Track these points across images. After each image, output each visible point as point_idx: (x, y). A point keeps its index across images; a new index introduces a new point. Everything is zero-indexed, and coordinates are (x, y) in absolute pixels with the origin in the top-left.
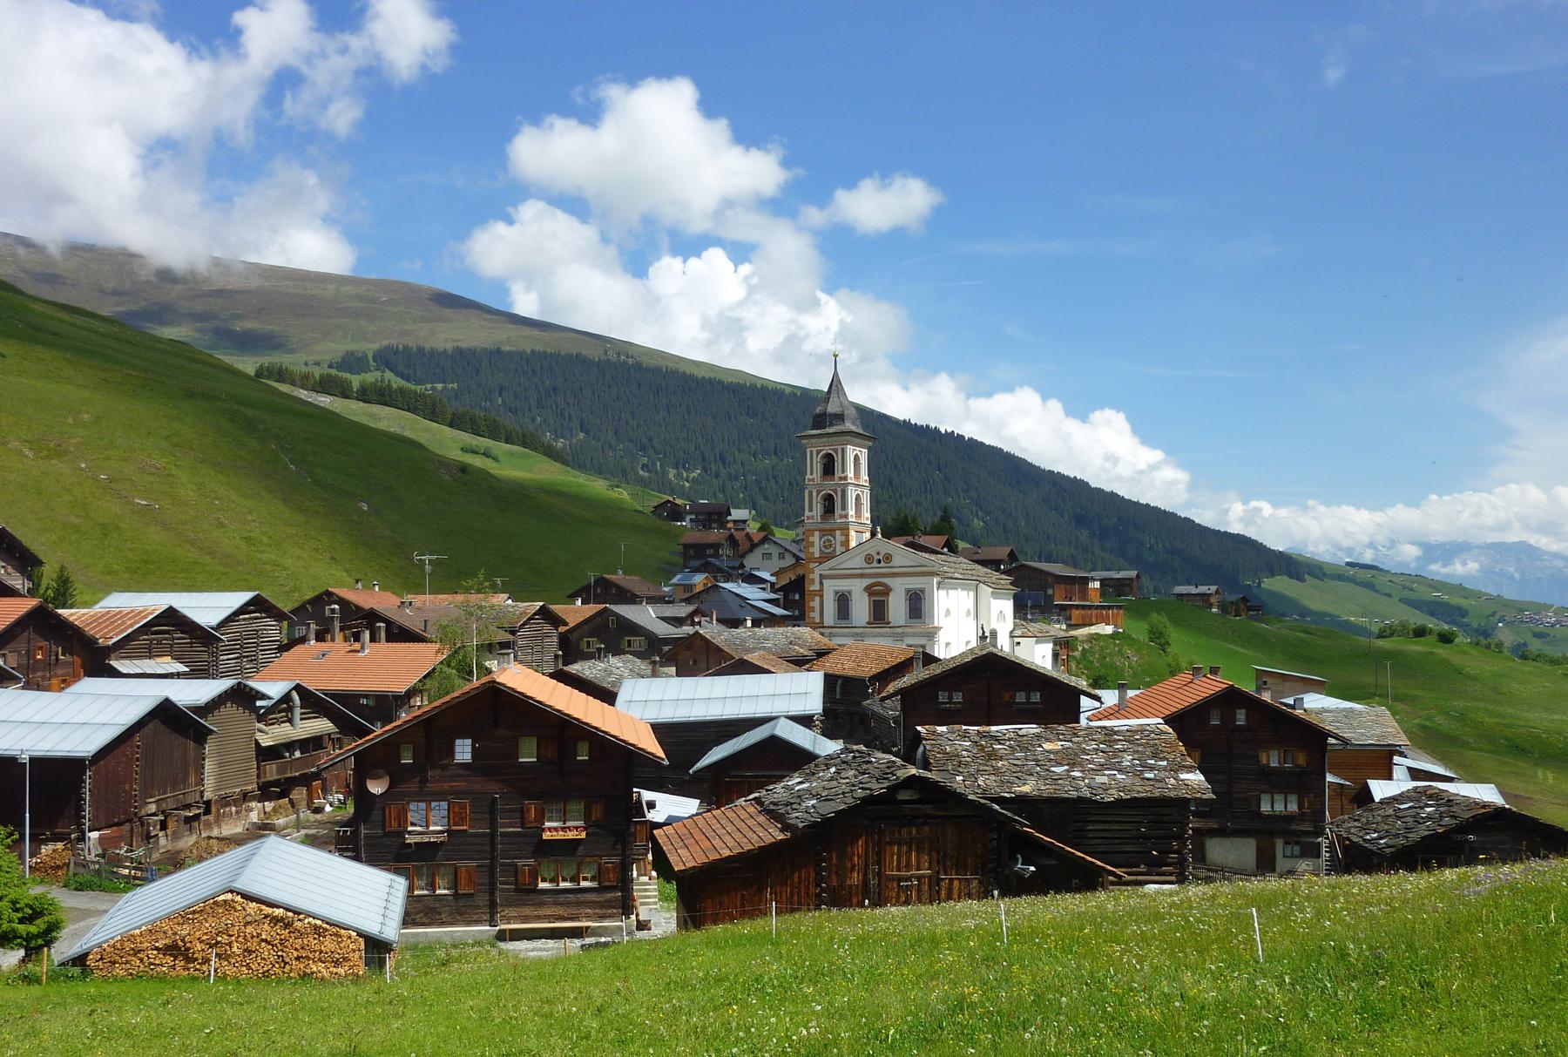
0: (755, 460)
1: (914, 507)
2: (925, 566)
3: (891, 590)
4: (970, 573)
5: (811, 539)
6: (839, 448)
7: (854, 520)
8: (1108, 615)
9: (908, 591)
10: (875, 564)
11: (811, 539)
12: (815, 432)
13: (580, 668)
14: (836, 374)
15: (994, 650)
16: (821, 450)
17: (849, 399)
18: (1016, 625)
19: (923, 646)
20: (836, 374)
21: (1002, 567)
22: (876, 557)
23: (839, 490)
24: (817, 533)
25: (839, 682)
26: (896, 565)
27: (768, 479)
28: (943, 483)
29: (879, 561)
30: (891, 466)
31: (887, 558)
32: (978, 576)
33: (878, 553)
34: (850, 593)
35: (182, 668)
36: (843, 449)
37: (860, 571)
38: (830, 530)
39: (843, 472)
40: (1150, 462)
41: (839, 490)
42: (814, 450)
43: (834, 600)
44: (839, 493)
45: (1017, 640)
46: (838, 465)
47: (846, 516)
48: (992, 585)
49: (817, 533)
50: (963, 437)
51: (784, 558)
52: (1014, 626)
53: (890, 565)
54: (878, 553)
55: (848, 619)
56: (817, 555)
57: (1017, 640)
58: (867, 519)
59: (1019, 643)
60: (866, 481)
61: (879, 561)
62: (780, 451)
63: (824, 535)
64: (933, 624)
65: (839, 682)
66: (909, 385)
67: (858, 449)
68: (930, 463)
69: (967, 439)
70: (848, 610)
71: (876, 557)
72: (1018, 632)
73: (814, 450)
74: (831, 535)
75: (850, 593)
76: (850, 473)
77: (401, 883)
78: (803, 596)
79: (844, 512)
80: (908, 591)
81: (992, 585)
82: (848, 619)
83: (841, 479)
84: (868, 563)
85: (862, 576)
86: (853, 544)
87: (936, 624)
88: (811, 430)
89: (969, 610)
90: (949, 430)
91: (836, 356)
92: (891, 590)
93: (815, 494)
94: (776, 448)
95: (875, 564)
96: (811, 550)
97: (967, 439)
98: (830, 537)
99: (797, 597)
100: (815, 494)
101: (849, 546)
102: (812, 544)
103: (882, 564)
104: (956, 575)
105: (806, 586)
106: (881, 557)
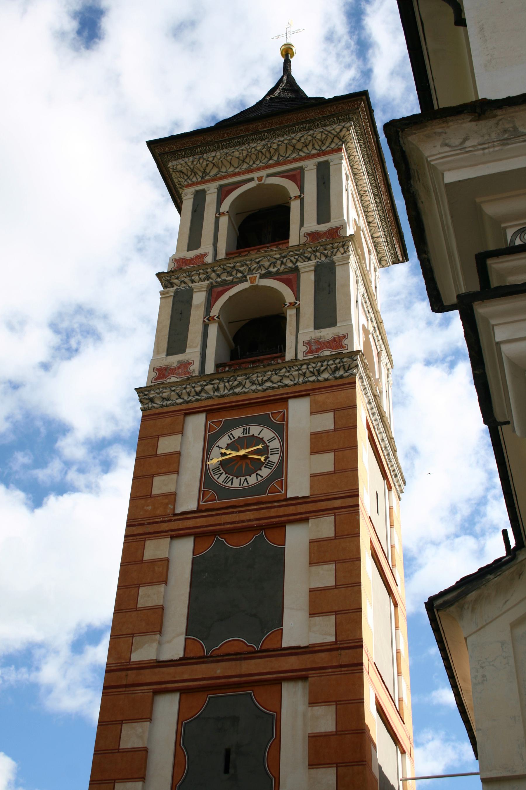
74: (265, 422)
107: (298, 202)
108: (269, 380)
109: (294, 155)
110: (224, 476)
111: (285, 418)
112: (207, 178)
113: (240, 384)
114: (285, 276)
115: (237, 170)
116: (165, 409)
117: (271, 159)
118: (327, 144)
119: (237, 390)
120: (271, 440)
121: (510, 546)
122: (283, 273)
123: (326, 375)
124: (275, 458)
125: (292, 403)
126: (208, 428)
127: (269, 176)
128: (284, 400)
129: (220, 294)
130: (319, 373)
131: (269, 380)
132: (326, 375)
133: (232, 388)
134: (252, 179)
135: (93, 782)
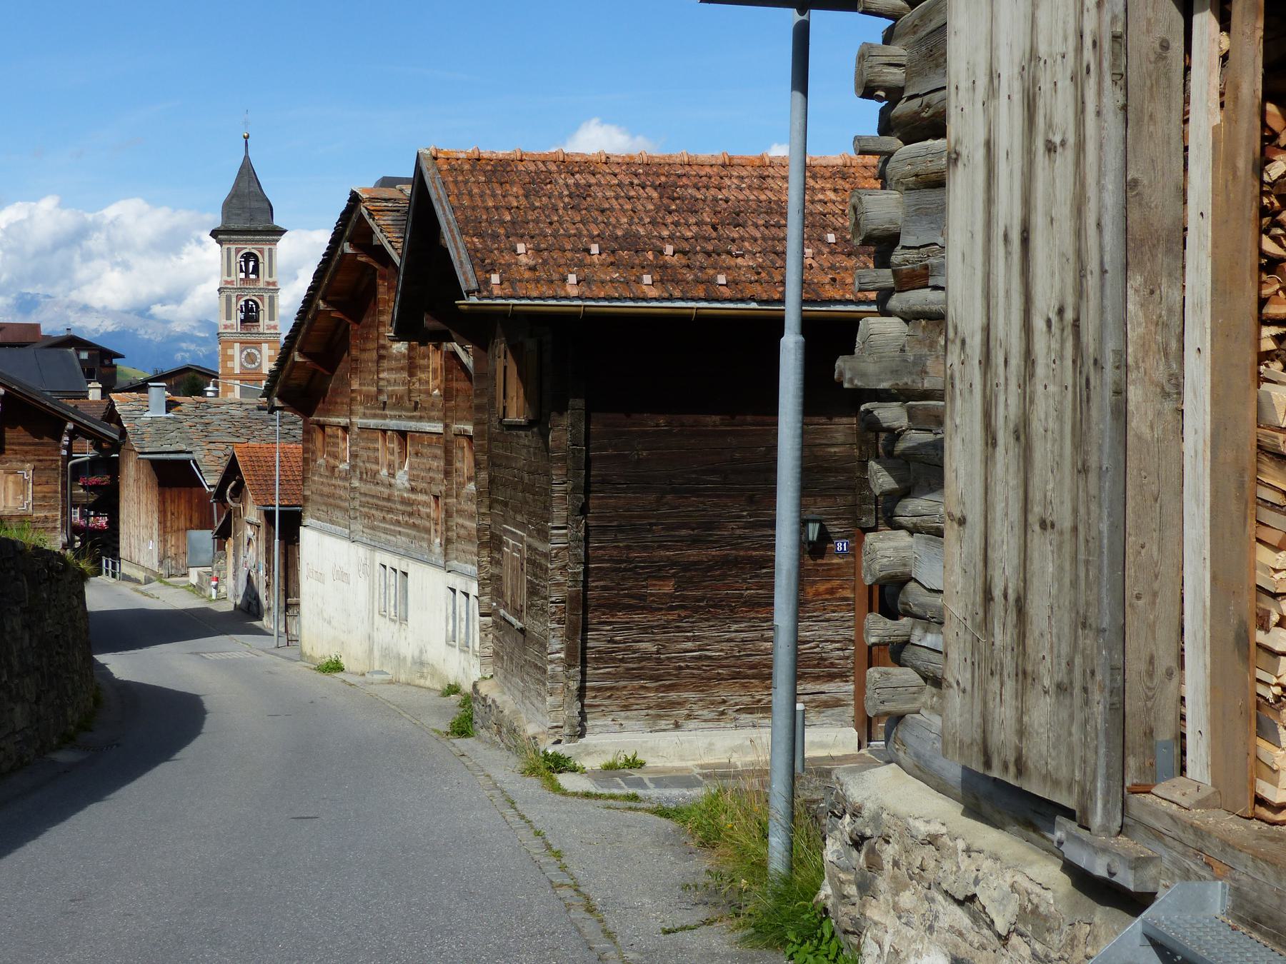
5: (230, 352)
6: (266, 248)
8: (577, 610)
11: (230, 352)
13: (385, 220)
14: (247, 158)
17: (896, 295)
20: (247, 158)
23: (266, 296)
35: (460, 307)
36: (270, 250)
39: (271, 276)
41: (266, 296)
44: (266, 254)
49: (237, 346)
56: (237, 371)
66: (912, 525)
73: (233, 247)
74: (255, 348)
77: (275, 223)
79: (272, 323)
91: (246, 138)
93: (234, 300)
96: (230, 364)
100: (234, 300)
102: (232, 358)
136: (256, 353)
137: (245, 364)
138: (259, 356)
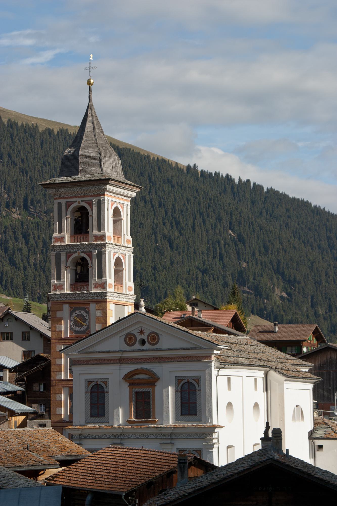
0: (312, 249)
1: (200, 275)
2: (201, 348)
3: (158, 379)
4: (259, 357)
5: (59, 314)
6: (95, 200)
7: (113, 290)
9: (89, 382)
10: (137, 346)
12: (65, 179)
15: (276, 456)
16: (123, 208)
18: (316, 423)
19: (199, 451)
21: (305, 350)
22: (139, 337)
24: (66, 307)
25: (89, 498)
26: (164, 347)
27: (16, 239)
28: (236, 245)
29: (143, 342)
30: (171, 224)
31: (153, 338)
32: (269, 361)
33: (142, 332)
34: (105, 382)
37: (119, 355)
38: (84, 303)
40: (273, 188)
42: (63, 202)
43: (86, 392)
45: (318, 443)
46: (94, 220)
47: (103, 285)
48: (286, 373)
49: (66, 307)
50: (261, 188)
51: (28, 338)
52: (315, 424)
53: (154, 347)
54: (142, 332)
55: (103, 416)
57: (318, 443)
58: (130, 288)
59: (321, 447)
60: (128, 241)
61: (143, 342)
62: (32, 203)
63: (75, 309)
64: (212, 422)
65: (89, 498)
67: (118, 201)
68: (219, 219)
69: (265, 190)
70: (104, 404)
71: (139, 337)
72: (320, 433)
73: (63, 202)
74: (84, 309)
75: (105, 382)
76: (109, 231)
78: (48, 387)
80: (89, 382)
81: (286, 373)
82: (103, 416)
83: (97, 238)
84: (129, 345)
85: (121, 361)
86: (111, 320)
87: (215, 422)
88: (60, 176)
89: (256, 405)
90: (244, 179)
92: (158, 379)
93: (63, 258)
94: (26, 200)
95: (137, 346)
97: (265, 190)
98: (82, 312)
99: (42, 389)
101: (106, 322)
103: (147, 346)
104: (240, 360)
105: (52, 374)
106: (145, 338)
107: (92, 217)
108: (85, 296)
109: (89, 194)
110: (75, 326)
111: (89, 309)
112: (61, 197)
113: (77, 297)
114: (88, 253)
115: (71, 196)
116: (57, 302)
117: (82, 193)
118: (100, 192)
119: (76, 298)
120: (86, 316)
121: (264, 190)
122: (88, 252)
123: (99, 298)
124: (87, 322)
125: (91, 304)
126: (70, 310)
127: (82, 201)
128: (89, 303)
129: (70, 256)
130: (98, 297)
131: (85, 296)
132: (99, 298)
133: (75, 297)
134: (76, 201)
135: (61, 505)
136: (85, 314)
137: (78, 329)
138: (87, 318)
